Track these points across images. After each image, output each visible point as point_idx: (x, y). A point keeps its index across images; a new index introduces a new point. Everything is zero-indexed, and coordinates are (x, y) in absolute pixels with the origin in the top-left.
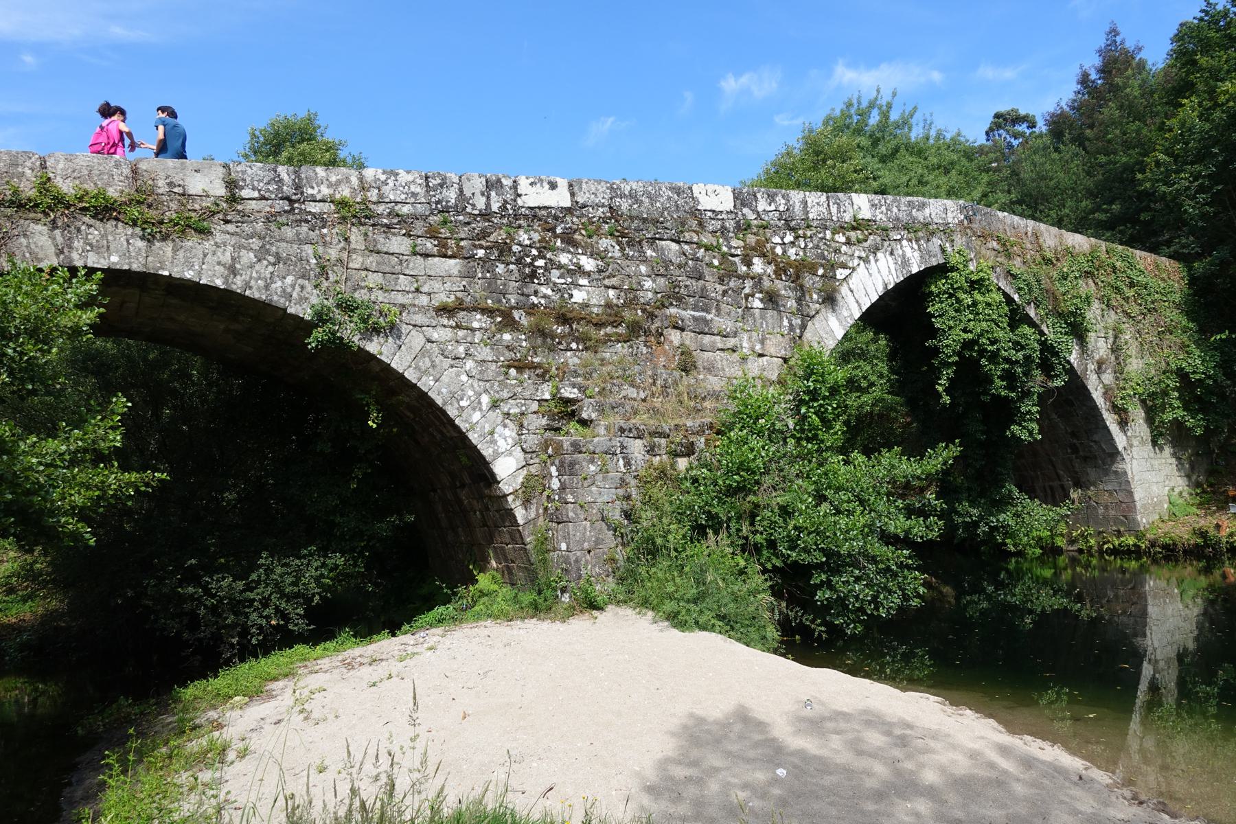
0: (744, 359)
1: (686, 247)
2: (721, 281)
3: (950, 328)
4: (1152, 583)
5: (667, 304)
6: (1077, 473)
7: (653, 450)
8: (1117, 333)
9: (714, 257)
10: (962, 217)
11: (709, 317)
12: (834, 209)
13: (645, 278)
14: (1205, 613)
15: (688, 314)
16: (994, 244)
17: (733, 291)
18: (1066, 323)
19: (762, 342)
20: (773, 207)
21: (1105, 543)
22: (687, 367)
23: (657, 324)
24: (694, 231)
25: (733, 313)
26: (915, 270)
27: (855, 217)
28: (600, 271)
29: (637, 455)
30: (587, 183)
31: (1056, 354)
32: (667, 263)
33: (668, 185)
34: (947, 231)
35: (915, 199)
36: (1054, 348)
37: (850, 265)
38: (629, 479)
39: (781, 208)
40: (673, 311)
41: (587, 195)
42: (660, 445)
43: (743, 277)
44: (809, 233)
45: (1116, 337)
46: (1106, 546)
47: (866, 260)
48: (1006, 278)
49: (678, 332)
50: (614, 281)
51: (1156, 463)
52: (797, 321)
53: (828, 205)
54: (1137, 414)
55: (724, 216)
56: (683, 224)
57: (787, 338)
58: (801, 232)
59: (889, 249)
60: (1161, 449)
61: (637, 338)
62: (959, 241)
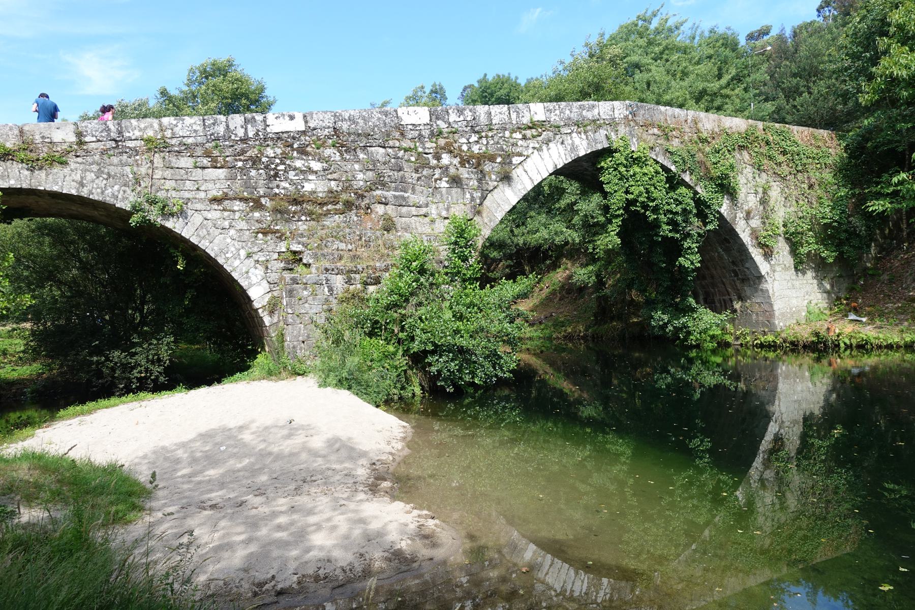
0: (433, 221)
1: (390, 150)
2: (417, 171)
3: (615, 191)
5: (374, 188)
6: (738, 290)
9: (412, 155)
10: (628, 113)
11: (406, 195)
12: (514, 116)
14: (834, 390)
15: (390, 194)
16: (656, 131)
17: (426, 177)
18: (716, 185)
19: (448, 210)
20: (462, 118)
21: (756, 340)
23: (366, 201)
24: (397, 140)
25: (425, 192)
26: (582, 153)
27: (531, 120)
28: (324, 170)
29: (337, 284)
31: (709, 207)
32: (375, 162)
34: (613, 124)
36: (707, 202)
37: (525, 153)
38: (331, 299)
39: (469, 119)
40: (378, 192)
41: (317, 121)
42: (355, 278)
43: (434, 168)
44: (490, 134)
45: (765, 192)
46: (756, 342)
47: (539, 149)
48: (664, 155)
49: (383, 206)
50: (335, 176)
51: (797, 283)
52: (478, 195)
53: (509, 113)
54: (782, 249)
55: (421, 127)
56: (388, 135)
57: (469, 206)
58: (483, 134)
59: (561, 140)
60: (804, 273)
61: (350, 211)
62: (623, 130)
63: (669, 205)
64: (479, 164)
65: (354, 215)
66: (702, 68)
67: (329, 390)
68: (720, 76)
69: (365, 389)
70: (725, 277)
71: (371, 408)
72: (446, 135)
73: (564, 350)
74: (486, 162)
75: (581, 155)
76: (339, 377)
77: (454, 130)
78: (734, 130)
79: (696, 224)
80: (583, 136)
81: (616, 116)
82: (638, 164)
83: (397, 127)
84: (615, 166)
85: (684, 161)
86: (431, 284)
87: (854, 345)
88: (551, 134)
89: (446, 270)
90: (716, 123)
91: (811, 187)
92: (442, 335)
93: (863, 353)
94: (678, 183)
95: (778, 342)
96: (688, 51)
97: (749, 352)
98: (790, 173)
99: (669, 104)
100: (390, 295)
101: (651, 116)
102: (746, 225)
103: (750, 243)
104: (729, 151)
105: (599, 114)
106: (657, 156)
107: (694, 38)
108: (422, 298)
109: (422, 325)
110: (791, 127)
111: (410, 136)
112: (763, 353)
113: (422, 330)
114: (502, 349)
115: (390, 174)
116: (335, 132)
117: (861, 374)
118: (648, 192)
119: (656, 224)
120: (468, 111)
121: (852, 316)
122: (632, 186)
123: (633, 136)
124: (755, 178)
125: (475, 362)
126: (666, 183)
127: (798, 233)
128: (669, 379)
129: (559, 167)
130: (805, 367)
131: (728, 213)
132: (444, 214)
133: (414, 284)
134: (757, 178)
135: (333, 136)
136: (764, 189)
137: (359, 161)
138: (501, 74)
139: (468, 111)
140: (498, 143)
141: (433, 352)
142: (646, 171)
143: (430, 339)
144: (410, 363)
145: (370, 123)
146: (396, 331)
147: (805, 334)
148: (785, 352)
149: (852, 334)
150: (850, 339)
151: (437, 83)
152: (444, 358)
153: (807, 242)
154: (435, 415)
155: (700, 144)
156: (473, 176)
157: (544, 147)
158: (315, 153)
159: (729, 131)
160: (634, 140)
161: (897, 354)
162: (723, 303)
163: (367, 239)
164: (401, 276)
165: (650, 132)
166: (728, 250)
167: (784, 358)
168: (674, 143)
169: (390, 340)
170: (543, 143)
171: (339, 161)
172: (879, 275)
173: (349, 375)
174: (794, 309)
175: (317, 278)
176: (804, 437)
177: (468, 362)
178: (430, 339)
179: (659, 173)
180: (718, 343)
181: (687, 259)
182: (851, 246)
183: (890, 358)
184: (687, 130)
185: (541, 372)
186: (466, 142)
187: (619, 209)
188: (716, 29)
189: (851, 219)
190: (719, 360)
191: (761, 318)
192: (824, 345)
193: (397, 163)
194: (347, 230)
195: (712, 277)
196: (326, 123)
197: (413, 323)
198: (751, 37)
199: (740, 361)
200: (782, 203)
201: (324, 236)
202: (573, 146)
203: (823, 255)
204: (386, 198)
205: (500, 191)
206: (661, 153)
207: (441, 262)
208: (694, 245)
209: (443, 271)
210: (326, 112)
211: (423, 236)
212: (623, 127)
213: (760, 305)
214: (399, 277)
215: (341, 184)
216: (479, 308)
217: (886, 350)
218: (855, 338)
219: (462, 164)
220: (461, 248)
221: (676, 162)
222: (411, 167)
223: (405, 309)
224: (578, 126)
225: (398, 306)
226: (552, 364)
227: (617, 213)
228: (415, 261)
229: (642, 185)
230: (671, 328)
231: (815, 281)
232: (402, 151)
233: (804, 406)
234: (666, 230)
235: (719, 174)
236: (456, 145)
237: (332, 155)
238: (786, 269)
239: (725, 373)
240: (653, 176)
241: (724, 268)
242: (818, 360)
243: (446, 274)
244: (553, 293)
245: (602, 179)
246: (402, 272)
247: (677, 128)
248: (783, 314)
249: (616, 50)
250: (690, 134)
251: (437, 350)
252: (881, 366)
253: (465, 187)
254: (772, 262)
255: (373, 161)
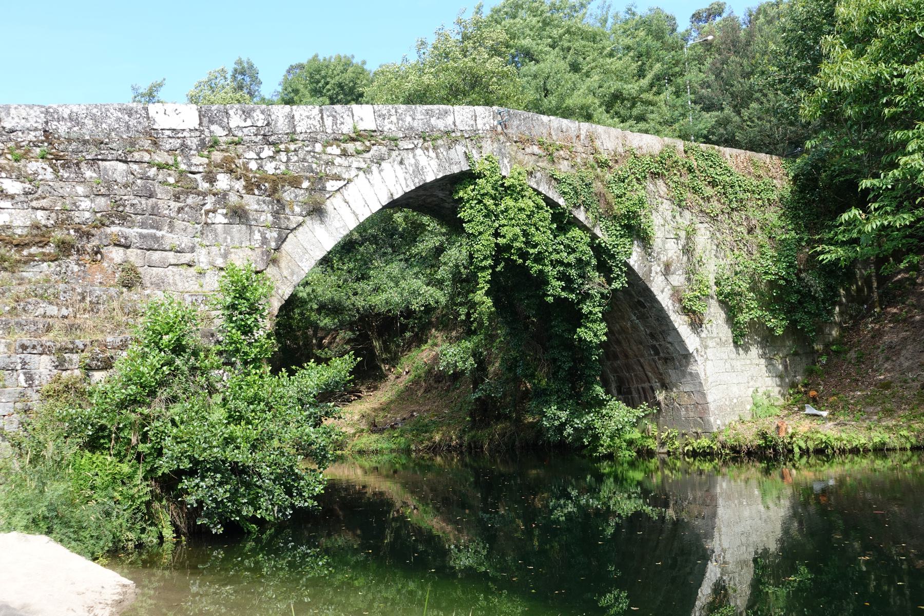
0: (201, 273)
1: (135, 167)
2: (177, 198)
3: (480, 233)
4: (724, 485)
5: (107, 222)
6: (661, 374)
7: (63, 365)
8: (690, 235)
9: (170, 175)
10: (496, 123)
11: (159, 234)
12: (328, 122)
13: (82, 199)
14: (795, 515)
15: (133, 232)
16: (536, 149)
17: (191, 207)
18: (621, 226)
19: (225, 256)
20: (249, 123)
21: (687, 445)
22: (130, 280)
23: (95, 242)
24: (147, 151)
25: (189, 230)
26: (430, 178)
27: (355, 128)
28: (26, 194)
29: (41, 370)
30: (16, 108)
31: (612, 257)
32: (109, 184)
33: (117, 107)
34: (474, 137)
35: (435, 107)
36: (610, 250)
37: (346, 176)
38: (29, 392)
39: (259, 124)
40: (114, 229)
41: (17, 120)
42: (71, 360)
43: (204, 194)
44: (292, 147)
45: (688, 238)
46: (686, 448)
47: (367, 171)
48: (549, 183)
49: (121, 250)
50: (43, 203)
51: (738, 364)
52: (272, 235)
53: (322, 118)
54: (715, 314)
55: (186, 134)
56: (133, 144)
57: (258, 251)
58: (282, 147)
59: (399, 159)
60: (747, 350)
61: (68, 256)
62: (489, 147)
63: (558, 253)
64: (275, 190)
65: (73, 263)
66: (615, 64)
67: (14, 536)
68: (641, 74)
69: (75, 532)
70: (643, 356)
71: (84, 563)
72: (225, 147)
73: (429, 468)
74: (286, 188)
75: (428, 181)
76: (33, 515)
77: (236, 139)
78: (644, 151)
79: (597, 280)
80: (432, 153)
81: (479, 127)
82: (512, 195)
83: (147, 132)
84: (479, 197)
85: (576, 193)
86: (193, 369)
87: (811, 449)
88: (384, 150)
89: (219, 347)
90: (620, 142)
91: (750, 231)
92: (206, 446)
93: (824, 461)
94: (569, 223)
95: (715, 447)
96: (598, 38)
97: (679, 464)
98: (723, 212)
99: (567, 113)
100: (125, 386)
101: (529, 129)
102: (665, 282)
103: (671, 308)
104: (638, 179)
105: (454, 123)
106: (538, 184)
107: (606, 21)
108: (176, 389)
109: (175, 430)
110: (721, 148)
111: (168, 147)
112: (697, 463)
113: (175, 438)
114: (301, 465)
115: (134, 202)
116: (47, 137)
117: (825, 491)
118: (525, 234)
119: (542, 280)
120: (258, 112)
121: (810, 410)
122: (504, 225)
123: (503, 156)
124: (674, 217)
125: (260, 487)
126: (553, 221)
127: (735, 294)
128: (571, 508)
129: (396, 197)
130: (753, 482)
131: (639, 266)
132: (220, 262)
133: (165, 368)
134: (678, 217)
135: (42, 142)
136: (688, 233)
137: (83, 182)
138: (342, 55)
139: (258, 112)
140: (304, 160)
141: (191, 473)
142: (523, 206)
143: (186, 452)
144: (158, 491)
145: (104, 126)
146: (134, 441)
147: (749, 436)
148: (724, 462)
149: (809, 434)
150: (806, 441)
151: (244, 59)
152: (209, 481)
153: (747, 307)
154: (194, 570)
155: (599, 170)
156: (265, 208)
157: (374, 168)
158: (11, 167)
159: (638, 153)
160: (506, 161)
161: (865, 461)
162: (641, 390)
163: (95, 300)
164: (144, 356)
165: (528, 150)
166: (643, 317)
167: (725, 470)
168: (561, 167)
169: (125, 456)
170: (372, 161)
171: (52, 180)
172: (846, 352)
173: (49, 510)
174: (735, 401)
175: (8, 360)
176: (756, 584)
177: (249, 486)
178: (186, 452)
179: (542, 208)
180: (638, 452)
181: (590, 329)
182: (806, 313)
183: (856, 467)
184: (580, 149)
185: (398, 504)
186: (256, 157)
187: (485, 258)
188: (633, 9)
189: (803, 275)
190: (638, 475)
191: (692, 414)
192: (775, 450)
193: (145, 186)
194: (62, 286)
195: (626, 356)
196: (31, 123)
197: (161, 429)
198: (697, 17)
199: (667, 476)
200: (714, 252)
201: (22, 295)
202: (417, 167)
203: (769, 324)
204: (126, 238)
205: (307, 229)
206: (544, 180)
207: (212, 335)
208: (597, 309)
209: (214, 348)
210: (31, 107)
211: (186, 295)
212: (489, 142)
213: (689, 395)
214: (142, 357)
215: (53, 215)
216: (267, 404)
217: (850, 456)
218: (812, 439)
219: (249, 189)
220: (241, 313)
221: (564, 193)
222: (168, 192)
223: (150, 407)
224: (424, 139)
225: (139, 402)
226: (412, 487)
227: (484, 263)
228: (167, 334)
229: (517, 225)
230: (569, 430)
231: (763, 361)
232: (155, 169)
233: (754, 538)
234: (556, 287)
235: (624, 211)
236: (239, 162)
237: (40, 171)
238: (722, 343)
239: (645, 493)
240: (533, 211)
241: (641, 343)
242: (767, 472)
243: (220, 353)
244: (416, 382)
245: (461, 215)
246: (146, 350)
247: (565, 146)
248: (720, 408)
249: (498, 34)
250: (584, 155)
251: (197, 469)
252: (848, 479)
253: (253, 223)
254: (703, 335)
255: (107, 182)
